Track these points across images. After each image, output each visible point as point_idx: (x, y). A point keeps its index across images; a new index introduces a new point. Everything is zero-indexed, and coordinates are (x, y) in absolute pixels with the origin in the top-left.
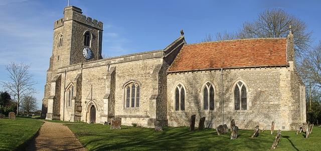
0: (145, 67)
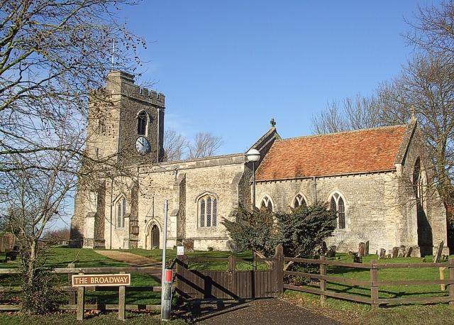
0: (223, 175)
